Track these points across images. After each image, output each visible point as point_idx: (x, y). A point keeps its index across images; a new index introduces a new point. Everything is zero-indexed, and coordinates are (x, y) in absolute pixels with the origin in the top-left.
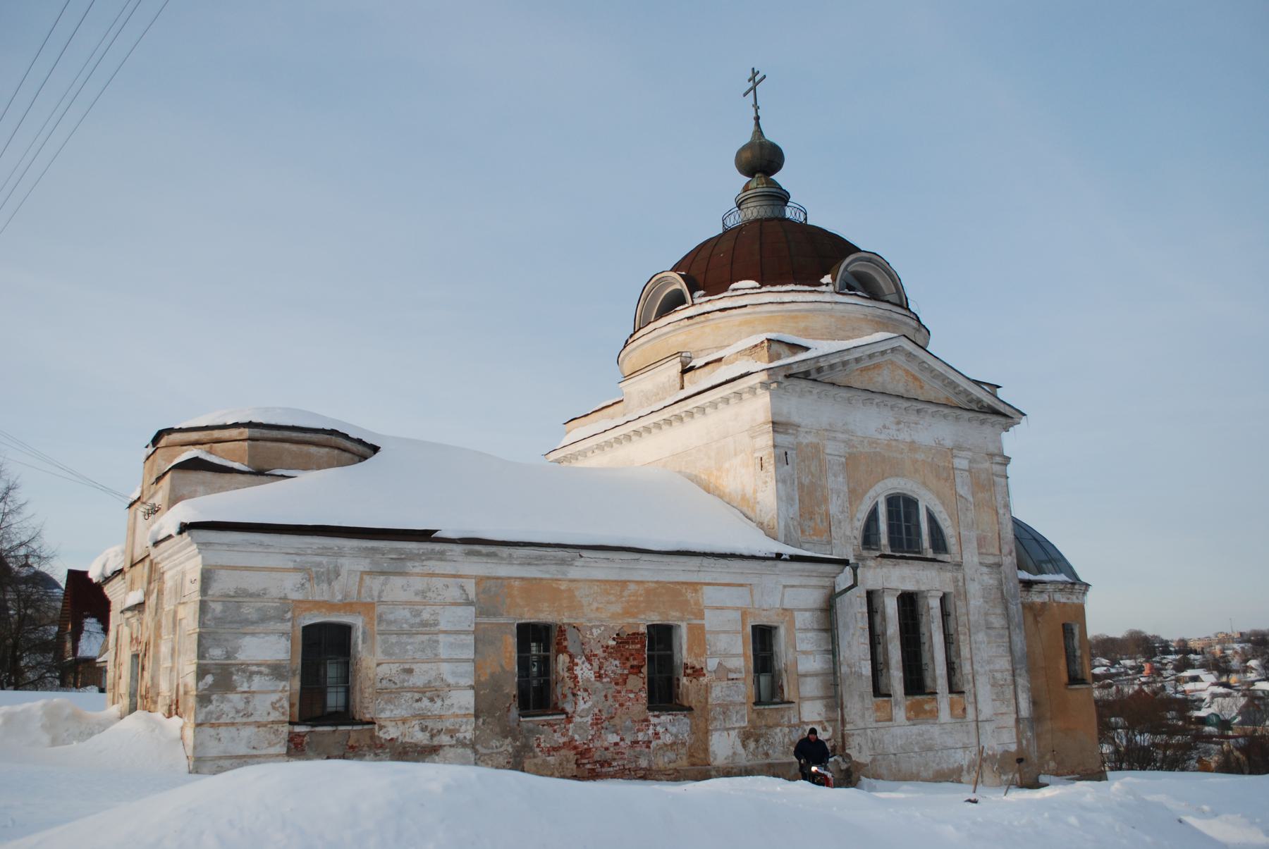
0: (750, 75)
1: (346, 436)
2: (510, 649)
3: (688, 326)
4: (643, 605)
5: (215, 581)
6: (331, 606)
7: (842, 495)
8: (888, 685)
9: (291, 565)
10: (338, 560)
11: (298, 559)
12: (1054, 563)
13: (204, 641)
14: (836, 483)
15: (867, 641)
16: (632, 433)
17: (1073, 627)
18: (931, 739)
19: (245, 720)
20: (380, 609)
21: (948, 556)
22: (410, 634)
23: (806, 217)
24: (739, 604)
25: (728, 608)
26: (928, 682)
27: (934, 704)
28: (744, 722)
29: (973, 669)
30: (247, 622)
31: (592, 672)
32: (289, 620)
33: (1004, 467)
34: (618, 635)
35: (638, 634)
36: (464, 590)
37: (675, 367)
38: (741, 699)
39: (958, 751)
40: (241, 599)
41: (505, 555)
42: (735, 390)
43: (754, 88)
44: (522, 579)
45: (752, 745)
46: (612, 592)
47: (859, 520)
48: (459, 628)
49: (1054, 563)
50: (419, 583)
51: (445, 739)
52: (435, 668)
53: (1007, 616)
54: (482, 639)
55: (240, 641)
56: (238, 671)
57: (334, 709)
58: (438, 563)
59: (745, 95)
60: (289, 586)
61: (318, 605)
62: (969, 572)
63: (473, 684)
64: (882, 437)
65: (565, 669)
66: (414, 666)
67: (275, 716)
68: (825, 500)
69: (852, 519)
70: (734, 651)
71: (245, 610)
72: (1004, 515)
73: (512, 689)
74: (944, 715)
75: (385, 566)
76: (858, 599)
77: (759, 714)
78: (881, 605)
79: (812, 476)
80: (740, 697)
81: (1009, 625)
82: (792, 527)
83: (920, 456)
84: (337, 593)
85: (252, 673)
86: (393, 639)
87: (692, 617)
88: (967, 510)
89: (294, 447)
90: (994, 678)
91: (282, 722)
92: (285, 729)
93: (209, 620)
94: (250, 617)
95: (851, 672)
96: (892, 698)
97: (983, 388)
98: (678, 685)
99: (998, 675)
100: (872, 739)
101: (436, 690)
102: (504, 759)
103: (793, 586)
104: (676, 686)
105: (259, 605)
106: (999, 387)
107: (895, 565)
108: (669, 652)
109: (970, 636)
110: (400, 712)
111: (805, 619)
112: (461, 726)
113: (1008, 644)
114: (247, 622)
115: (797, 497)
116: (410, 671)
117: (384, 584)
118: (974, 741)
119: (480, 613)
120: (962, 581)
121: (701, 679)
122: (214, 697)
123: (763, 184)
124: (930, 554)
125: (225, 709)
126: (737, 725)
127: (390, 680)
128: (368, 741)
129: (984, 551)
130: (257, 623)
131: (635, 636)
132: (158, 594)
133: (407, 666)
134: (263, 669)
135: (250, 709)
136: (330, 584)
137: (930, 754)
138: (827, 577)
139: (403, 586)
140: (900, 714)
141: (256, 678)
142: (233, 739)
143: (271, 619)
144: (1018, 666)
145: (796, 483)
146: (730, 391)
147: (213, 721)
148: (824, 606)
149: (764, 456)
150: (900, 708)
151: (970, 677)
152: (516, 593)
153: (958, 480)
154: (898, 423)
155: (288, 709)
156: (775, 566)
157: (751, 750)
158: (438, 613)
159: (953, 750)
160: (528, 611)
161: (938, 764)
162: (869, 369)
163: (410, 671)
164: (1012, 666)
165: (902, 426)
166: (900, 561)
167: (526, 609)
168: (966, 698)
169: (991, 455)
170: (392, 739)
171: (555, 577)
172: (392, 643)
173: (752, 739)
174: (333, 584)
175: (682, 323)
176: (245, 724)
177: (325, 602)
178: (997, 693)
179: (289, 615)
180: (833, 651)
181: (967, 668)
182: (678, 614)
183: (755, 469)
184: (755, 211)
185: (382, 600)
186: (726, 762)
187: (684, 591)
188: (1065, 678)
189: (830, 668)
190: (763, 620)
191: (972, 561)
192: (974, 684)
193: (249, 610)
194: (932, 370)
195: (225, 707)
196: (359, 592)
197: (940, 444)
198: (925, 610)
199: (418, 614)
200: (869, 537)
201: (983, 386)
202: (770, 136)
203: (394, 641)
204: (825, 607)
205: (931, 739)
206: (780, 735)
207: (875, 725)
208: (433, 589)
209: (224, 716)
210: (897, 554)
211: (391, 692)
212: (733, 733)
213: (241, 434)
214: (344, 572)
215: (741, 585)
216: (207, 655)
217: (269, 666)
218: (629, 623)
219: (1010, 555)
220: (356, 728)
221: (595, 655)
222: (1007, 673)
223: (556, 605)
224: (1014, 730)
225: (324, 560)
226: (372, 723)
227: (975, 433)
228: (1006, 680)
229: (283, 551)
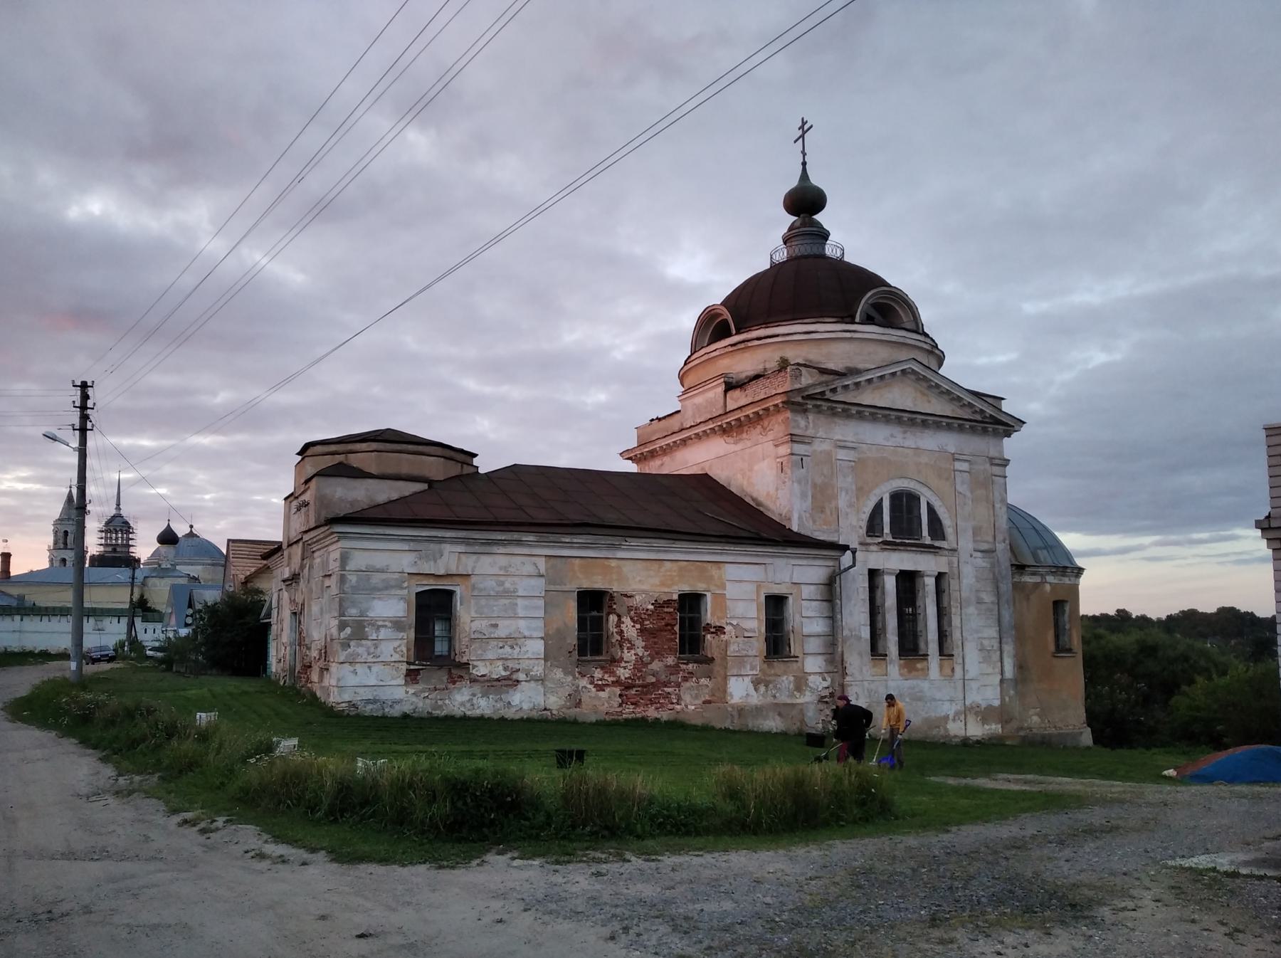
0: (800, 124)
8: (885, 647)
12: (1049, 549)
13: (344, 604)
14: (845, 482)
15: (868, 610)
21: (944, 542)
23: (843, 253)
26: (922, 645)
27: (925, 663)
28: (757, 670)
30: (376, 589)
32: (406, 588)
33: (1002, 468)
34: (656, 601)
35: (672, 600)
36: (537, 567)
38: (754, 653)
39: (945, 703)
43: (802, 136)
45: (762, 689)
49: (1049, 549)
51: (521, 676)
53: (998, 595)
56: (369, 625)
57: (440, 654)
59: (795, 142)
62: (964, 555)
63: (543, 635)
65: (614, 627)
67: (396, 657)
68: (835, 497)
69: (858, 512)
72: (1000, 508)
73: (572, 639)
76: (861, 576)
78: (882, 582)
79: (825, 477)
80: (754, 651)
82: (804, 519)
85: (379, 627)
86: (483, 602)
90: (982, 644)
92: (404, 667)
95: (852, 635)
96: (887, 658)
97: (983, 400)
98: (704, 639)
99: (986, 642)
100: (868, 690)
104: (702, 640)
106: (1003, 399)
109: (961, 609)
112: (533, 667)
113: (997, 616)
114: (376, 589)
116: (496, 626)
117: (476, 562)
119: (549, 582)
122: (352, 643)
124: (928, 541)
126: (751, 673)
129: (979, 538)
131: (668, 603)
132: (309, 569)
133: (493, 622)
134: (387, 623)
136: (435, 561)
137: (919, 703)
139: (490, 563)
141: (383, 630)
143: (392, 587)
145: (810, 483)
148: (827, 582)
150: (894, 666)
151: (960, 643)
153: (958, 480)
155: (406, 652)
157: (762, 692)
159: (941, 702)
161: (927, 713)
168: (955, 660)
174: (438, 561)
175: (727, 350)
179: (406, 585)
180: (833, 617)
181: (956, 635)
186: (741, 701)
187: (710, 568)
188: (1052, 647)
190: (777, 590)
192: (963, 648)
195: (361, 650)
199: (502, 584)
200: (873, 526)
201: (983, 398)
202: (816, 180)
206: (786, 682)
207: (871, 678)
208: (513, 565)
210: (898, 541)
211: (484, 640)
212: (747, 680)
216: (346, 613)
219: (1004, 542)
224: (999, 688)
228: (993, 646)
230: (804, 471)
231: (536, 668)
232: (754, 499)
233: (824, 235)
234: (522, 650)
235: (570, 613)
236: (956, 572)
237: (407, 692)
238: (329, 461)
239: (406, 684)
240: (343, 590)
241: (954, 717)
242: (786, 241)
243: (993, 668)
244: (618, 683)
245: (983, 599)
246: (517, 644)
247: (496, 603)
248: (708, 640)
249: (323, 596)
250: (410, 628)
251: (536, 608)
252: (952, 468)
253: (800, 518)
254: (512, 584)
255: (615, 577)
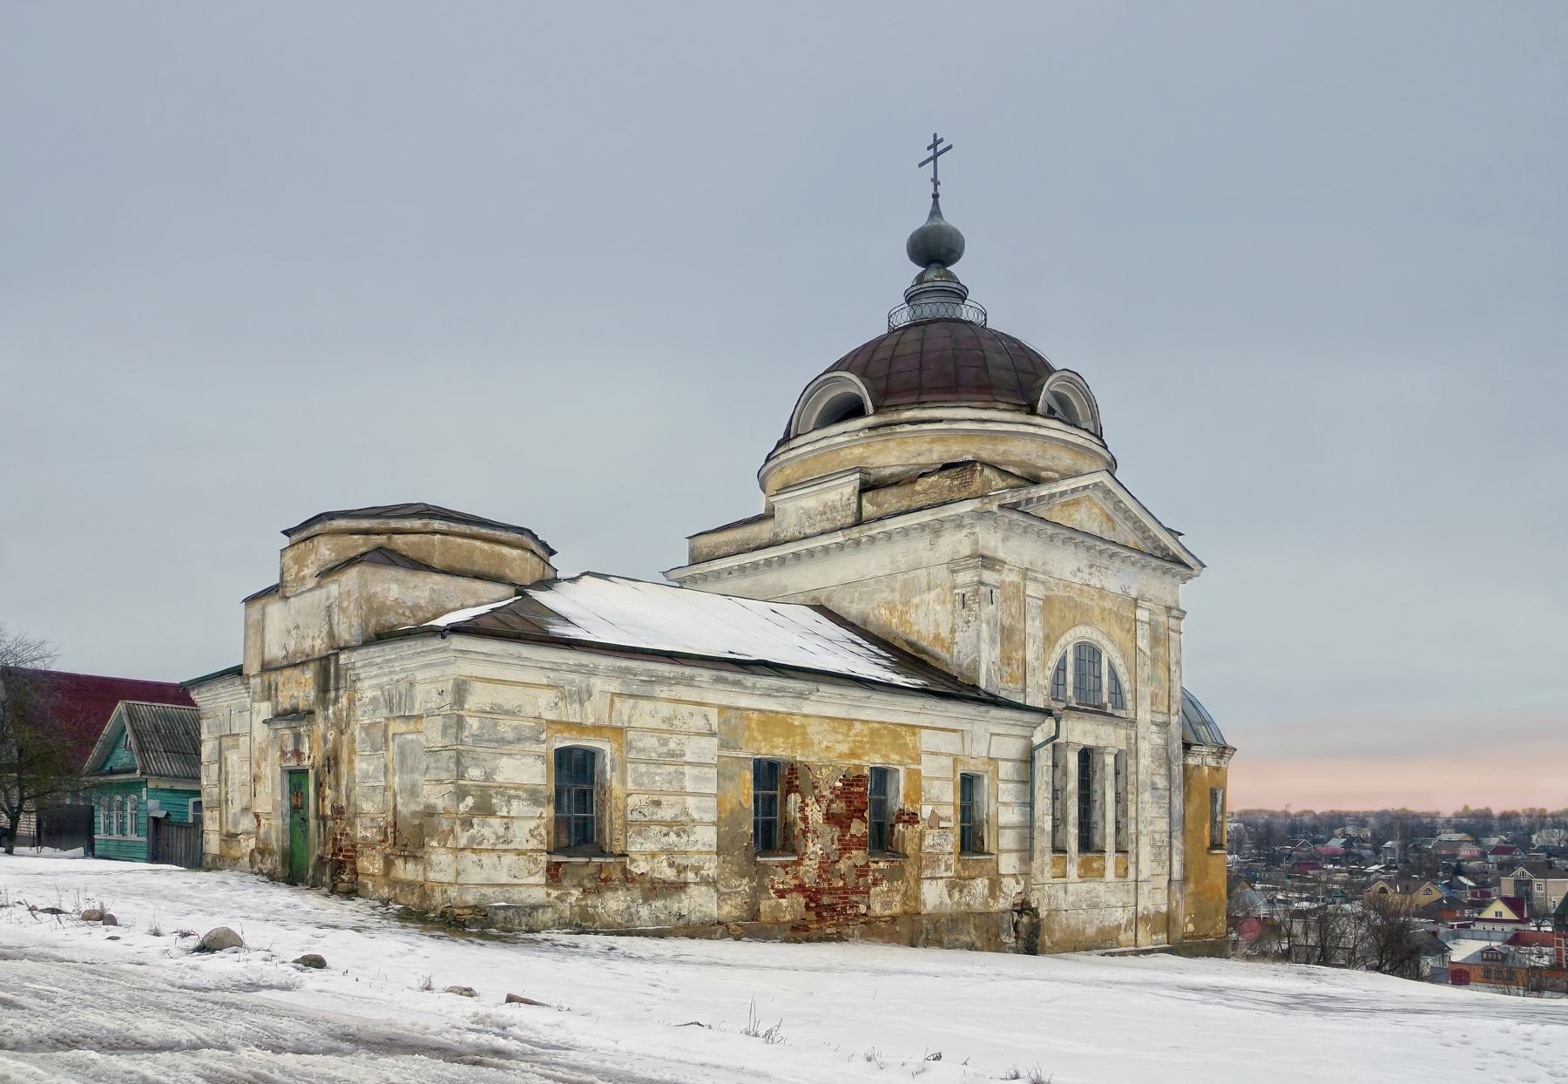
0: (932, 142)
1: (535, 537)
2: (748, 785)
3: (868, 437)
4: (868, 746)
5: (471, 693)
6: (580, 728)
7: (1037, 641)
9: (545, 681)
10: (591, 679)
11: (552, 675)
14: (1034, 627)
16: (791, 556)
17: (1217, 792)
18: (1097, 897)
19: (505, 847)
20: (631, 735)
21: (1123, 711)
22: (657, 764)
24: (952, 750)
25: (942, 754)
29: (1137, 829)
31: (821, 813)
32: (544, 741)
37: (850, 485)
38: (949, 848)
39: (1119, 909)
40: (495, 716)
41: (749, 685)
42: (938, 516)
43: (934, 158)
44: (760, 711)
45: (956, 895)
46: (840, 730)
47: (1049, 669)
48: (702, 760)
50: (665, 709)
51: (691, 876)
52: (681, 801)
53: (1170, 777)
54: (724, 775)
55: (498, 762)
58: (686, 689)
59: (921, 165)
60: (543, 704)
61: (569, 726)
62: (1141, 730)
64: (1076, 580)
66: (662, 799)
67: (534, 844)
70: (945, 800)
71: (501, 728)
74: (1110, 874)
75: (635, 689)
77: (964, 864)
78: (1063, 760)
79: (1013, 617)
81: (1170, 787)
83: (1107, 604)
84: (590, 716)
85: (510, 797)
87: (910, 761)
88: (1144, 664)
89: (486, 546)
91: (541, 851)
92: (544, 858)
93: (467, 737)
94: (506, 735)
99: (1157, 836)
101: (682, 825)
102: (742, 899)
103: (999, 735)
105: (515, 723)
107: (1079, 718)
108: (883, 797)
109: (1137, 796)
110: (650, 846)
111: (1006, 770)
114: (503, 741)
115: (999, 639)
116: (658, 804)
117: (633, 708)
118: (1133, 901)
119: (724, 745)
120: (1134, 739)
121: (916, 826)
122: (475, 821)
123: (942, 277)
125: (486, 834)
126: (945, 874)
127: (640, 812)
128: (620, 875)
129: (1155, 708)
130: (513, 742)
131: (859, 779)
135: (510, 836)
137: (1096, 911)
138: (1029, 727)
140: (1073, 871)
141: (515, 803)
142: (495, 867)
143: (527, 739)
144: (1176, 829)
145: (999, 624)
146: (931, 518)
147: (475, 847)
149: (967, 592)
151: (1134, 837)
152: (754, 726)
154: (1091, 566)
156: (988, 712)
158: (683, 744)
160: (765, 746)
162: (1070, 504)
163: (658, 804)
164: (1170, 828)
165: (1094, 569)
166: (1085, 714)
167: (763, 744)
169: (1169, 609)
170: (642, 874)
171: (791, 711)
172: (641, 773)
173: (957, 889)
176: (505, 851)
177: (575, 724)
178: (1155, 854)
179: (543, 737)
181: (1132, 829)
182: (897, 758)
183: (955, 607)
184: (934, 308)
185: (631, 725)
188: (1207, 843)
189: (1026, 821)
190: (970, 768)
191: (1145, 718)
193: (506, 727)
194: (1126, 511)
195: (486, 832)
196: (610, 716)
197: (1126, 593)
198: (1099, 767)
199: (665, 743)
202: (952, 217)
203: (643, 770)
204: (1024, 758)
205: (1097, 897)
206: (980, 885)
207: (1051, 880)
208: (679, 717)
209: (485, 841)
213: (426, 525)
214: (595, 691)
215: (954, 731)
216: (466, 775)
217: (526, 791)
218: (855, 765)
220: (608, 860)
221: (823, 797)
222: (1164, 834)
223: (790, 741)
224: (1166, 892)
225: (576, 677)
226: (624, 855)
227: (1152, 585)
229: (539, 665)
230: (993, 607)
231: (707, 864)
232: (911, 644)
233: (961, 295)
234: (691, 839)
235: (744, 791)
236: (1134, 749)
237: (548, 895)
238: (359, 544)
239: (548, 885)
240: (462, 740)
241: (1126, 927)
242: (910, 298)
243: (1163, 868)
244: (800, 888)
245: (1156, 784)
246: (684, 831)
247: (659, 771)
248: (899, 831)
249: (387, 747)
250: (549, 803)
251: (706, 779)
252: (1133, 617)
253: (988, 670)
254: (678, 744)
255: (798, 740)
